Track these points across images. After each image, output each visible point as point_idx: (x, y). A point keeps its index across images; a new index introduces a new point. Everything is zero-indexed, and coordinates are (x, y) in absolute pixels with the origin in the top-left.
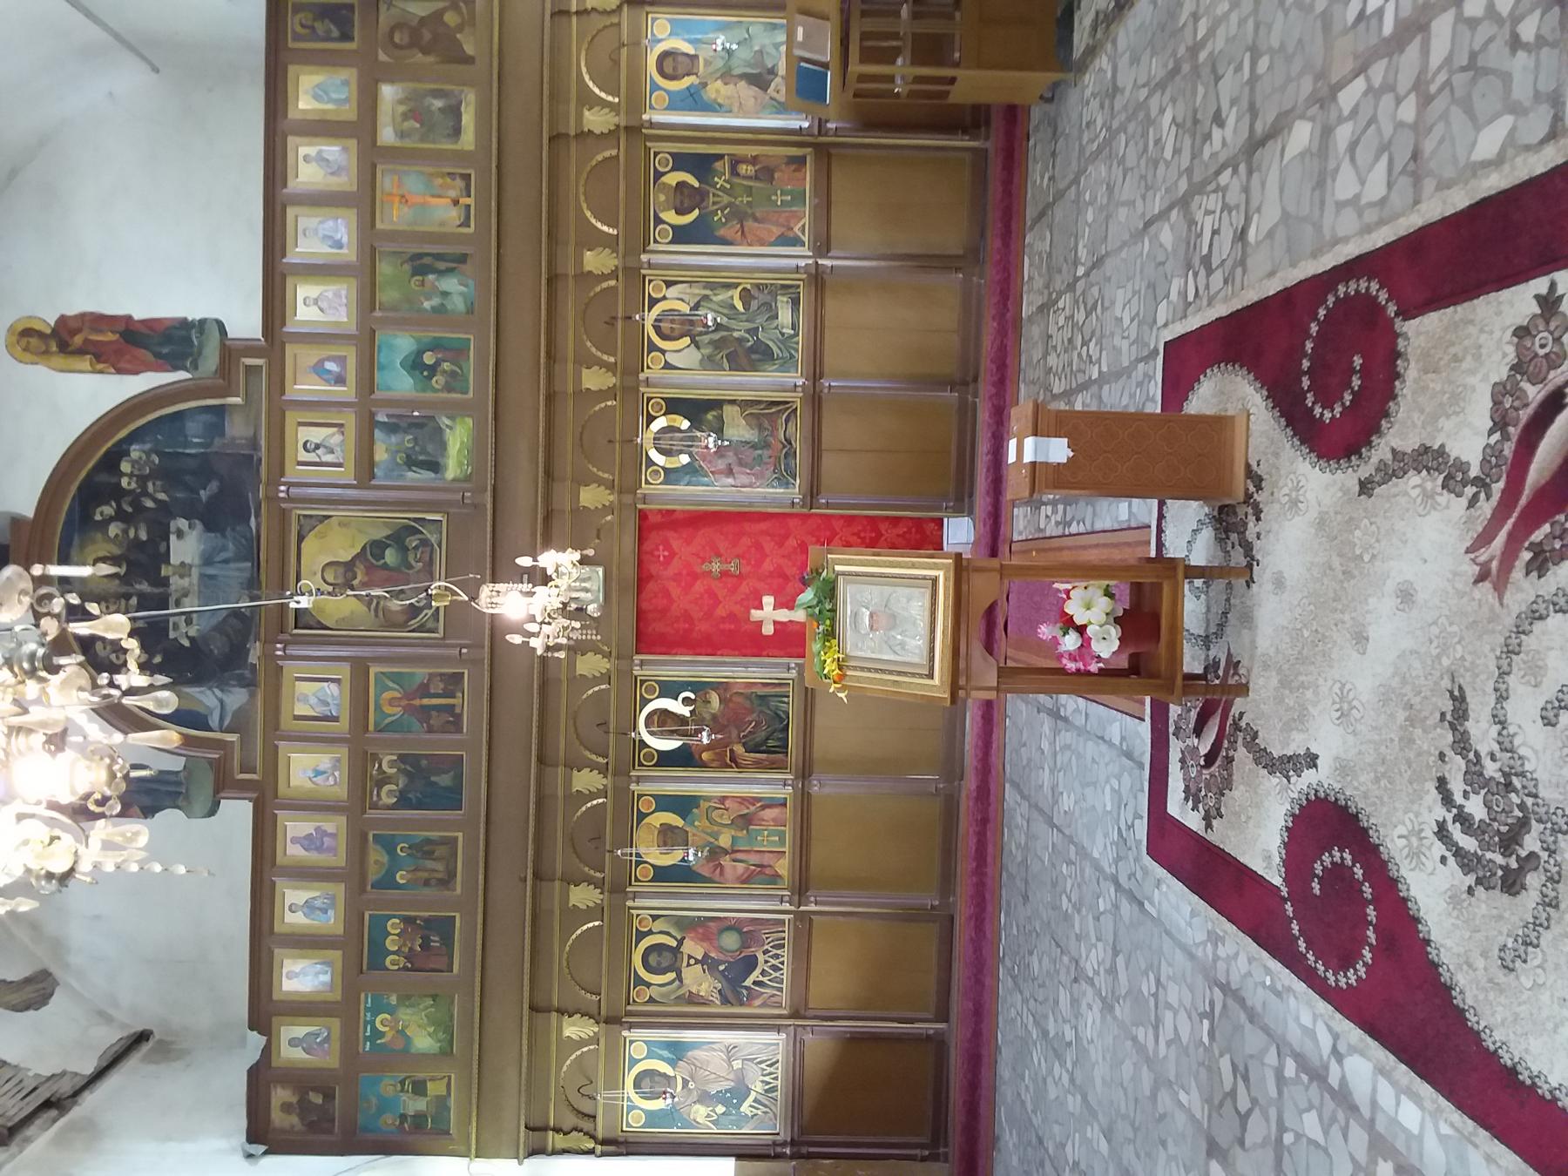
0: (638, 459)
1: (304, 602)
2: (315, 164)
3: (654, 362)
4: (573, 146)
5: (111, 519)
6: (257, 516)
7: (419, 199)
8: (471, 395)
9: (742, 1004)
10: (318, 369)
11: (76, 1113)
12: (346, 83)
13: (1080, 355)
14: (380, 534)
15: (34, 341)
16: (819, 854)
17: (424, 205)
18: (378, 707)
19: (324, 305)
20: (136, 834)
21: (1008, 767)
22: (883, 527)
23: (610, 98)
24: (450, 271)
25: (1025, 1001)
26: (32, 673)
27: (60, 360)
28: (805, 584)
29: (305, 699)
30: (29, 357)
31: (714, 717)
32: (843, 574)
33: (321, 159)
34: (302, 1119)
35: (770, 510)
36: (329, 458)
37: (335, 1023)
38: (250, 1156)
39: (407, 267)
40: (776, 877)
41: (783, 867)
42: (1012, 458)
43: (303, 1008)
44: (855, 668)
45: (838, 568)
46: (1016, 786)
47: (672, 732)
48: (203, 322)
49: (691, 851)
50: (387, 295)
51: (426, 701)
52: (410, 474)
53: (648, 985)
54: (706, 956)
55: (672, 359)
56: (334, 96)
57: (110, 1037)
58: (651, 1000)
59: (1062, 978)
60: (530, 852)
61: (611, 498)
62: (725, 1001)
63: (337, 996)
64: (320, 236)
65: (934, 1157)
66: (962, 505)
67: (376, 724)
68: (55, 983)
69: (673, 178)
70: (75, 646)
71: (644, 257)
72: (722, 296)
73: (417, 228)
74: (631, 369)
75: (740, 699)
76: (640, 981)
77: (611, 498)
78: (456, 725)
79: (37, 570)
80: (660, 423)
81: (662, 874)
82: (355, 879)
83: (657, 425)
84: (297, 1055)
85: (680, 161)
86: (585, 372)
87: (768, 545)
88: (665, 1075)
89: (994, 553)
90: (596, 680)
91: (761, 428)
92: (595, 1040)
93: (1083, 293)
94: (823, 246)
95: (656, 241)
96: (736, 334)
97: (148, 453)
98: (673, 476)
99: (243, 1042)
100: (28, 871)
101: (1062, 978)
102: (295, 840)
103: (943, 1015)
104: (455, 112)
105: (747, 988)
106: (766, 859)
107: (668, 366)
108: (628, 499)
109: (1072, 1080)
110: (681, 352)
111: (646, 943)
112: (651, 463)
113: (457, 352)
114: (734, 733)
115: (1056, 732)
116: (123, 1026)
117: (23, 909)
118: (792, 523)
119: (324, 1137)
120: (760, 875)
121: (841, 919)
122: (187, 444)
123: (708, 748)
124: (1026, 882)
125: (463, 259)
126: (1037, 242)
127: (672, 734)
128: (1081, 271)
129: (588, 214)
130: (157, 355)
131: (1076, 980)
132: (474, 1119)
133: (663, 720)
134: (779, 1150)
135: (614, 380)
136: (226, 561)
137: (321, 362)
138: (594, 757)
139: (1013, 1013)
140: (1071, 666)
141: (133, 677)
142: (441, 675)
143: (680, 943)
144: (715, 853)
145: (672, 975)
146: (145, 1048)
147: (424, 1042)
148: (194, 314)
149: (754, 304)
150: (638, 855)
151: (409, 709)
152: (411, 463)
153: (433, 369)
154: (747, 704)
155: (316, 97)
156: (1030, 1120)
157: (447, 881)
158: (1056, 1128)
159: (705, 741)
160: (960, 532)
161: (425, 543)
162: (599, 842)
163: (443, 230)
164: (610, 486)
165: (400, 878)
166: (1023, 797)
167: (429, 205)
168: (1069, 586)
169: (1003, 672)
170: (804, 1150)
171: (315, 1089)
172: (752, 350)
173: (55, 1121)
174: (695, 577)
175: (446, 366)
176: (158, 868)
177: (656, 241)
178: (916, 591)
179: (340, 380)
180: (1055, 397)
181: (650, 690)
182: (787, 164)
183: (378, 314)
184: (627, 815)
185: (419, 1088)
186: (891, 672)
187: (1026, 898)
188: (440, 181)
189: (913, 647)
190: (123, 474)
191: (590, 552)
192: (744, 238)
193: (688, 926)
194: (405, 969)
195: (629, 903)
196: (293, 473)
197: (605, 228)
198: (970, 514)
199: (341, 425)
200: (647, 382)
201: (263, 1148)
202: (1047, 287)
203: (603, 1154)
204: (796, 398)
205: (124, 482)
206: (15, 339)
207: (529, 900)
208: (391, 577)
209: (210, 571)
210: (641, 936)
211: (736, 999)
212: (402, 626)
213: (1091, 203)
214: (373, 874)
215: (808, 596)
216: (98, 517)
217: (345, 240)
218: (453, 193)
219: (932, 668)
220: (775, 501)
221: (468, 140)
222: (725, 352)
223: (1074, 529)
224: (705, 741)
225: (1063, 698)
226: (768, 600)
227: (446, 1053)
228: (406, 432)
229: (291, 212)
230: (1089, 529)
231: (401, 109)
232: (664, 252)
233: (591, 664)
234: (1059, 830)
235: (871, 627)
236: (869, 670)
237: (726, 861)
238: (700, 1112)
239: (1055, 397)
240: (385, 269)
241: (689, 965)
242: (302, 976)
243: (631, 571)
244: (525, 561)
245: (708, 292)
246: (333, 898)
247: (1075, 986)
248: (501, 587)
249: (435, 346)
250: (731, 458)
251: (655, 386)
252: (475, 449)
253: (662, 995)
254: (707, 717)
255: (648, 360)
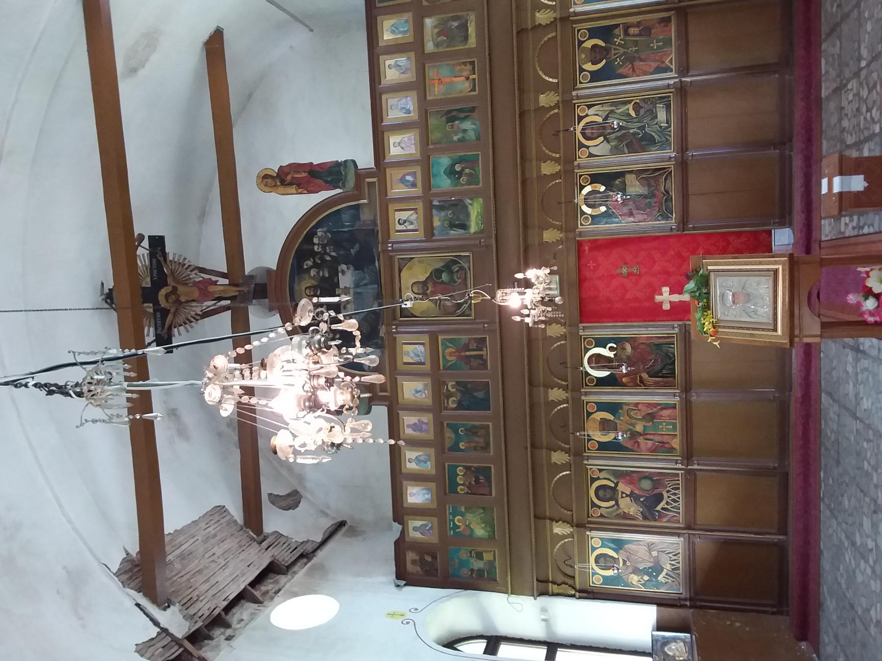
0: (574, 212)
1: (409, 304)
2: (394, 69)
3: (582, 154)
4: (530, 35)
5: (311, 267)
6: (379, 260)
7: (448, 80)
8: (481, 185)
9: (655, 520)
10: (403, 180)
11: (315, 560)
12: (407, 21)
13: (865, 118)
14: (439, 265)
15: (269, 181)
16: (698, 436)
17: (451, 82)
18: (444, 357)
19: (403, 145)
20: (367, 424)
21: (823, 383)
22: (731, 239)
23: (550, 3)
24: (466, 118)
25: (839, 524)
26: (319, 350)
27: (281, 189)
28: (689, 279)
29: (408, 354)
30: (268, 189)
31: (629, 358)
32: (714, 271)
33: (397, 66)
34: (422, 569)
35: (657, 234)
36: (411, 227)
37: (435, 520)
38: (398, 586)
39: (444, 118)
40: (672, 450)
41: (676, 443)
42: (824, 190)
43: (418, 512)
44: (724, 327)
45: (709, 268)
46: (830, 395)
47: (604, 367)
48: (346, 161)
49: (620, 434)
50: (435, 136)
51: (468, 353)
52: (452, 232)
53: (599, 507)
54: (632, 492)
55: (593, 151)
56: (402, 30)
57: (327, 524)
58: (602, 516)
59: (865, 510)
60: (528, 433)
61: (561, 235)
62: (645, 518)
63: (434, 506)
64: (400, 107)
65: (780, 613)
66: (784, 221)
67: (444, 366)
68: (301, 497)
69: (589, 44)
70: (300, 331)
71: (574, 93)
72: (622, 109)
73: (449, 96)
74: (569, 161)
75: (642, 346)
76: (594, 505)
77: (561, 235)
78: (484, 365)
79: (315, 300)
80: (588, 189)
81: (603, 446)
82: (441, 447)
83: (585, 191)
84: (417, 535)
85: (593, 33)
86: (543, 165)
87: (657, 255)
88: (612, 557)
89: (808, 251)
90: (558, 339)
91: (649, 186)
92: (571, 535)
93: (866, 78)
94: (684, 70)
95: (581, 83)
96: (631, 131)
97: (325, 232)
98: (597, 219)
99: (390, 528)
100: (323, 442)
101: (865, 510)
102: (408, 426)
103: (783, 529)
104: (464, 27)
105: (658, 511)
106: (665, 439)
107: (591, 155)
108: (571, 235)
109: (874, 572)
110: (599, 146)
111: (597, 484)
112: (583, 213)
113: (470, 162)
114: (641, 367)
115: (857, 360)
116: (333, 518)
117: (324, 461)
118: (672, 240)
119: (434, 578)
120: (662, 448)
121: (714, 474)
122: (343, 226)
123: (626, 375)
124: (838, 453)
125: (473, 109)
126: (830, 49)
127: (603, 368)
128: (863, 64)
129: (541, 73)
130: (326, 182)
131: (875, 512)
132: (509, 574)
133: (598, 361)
134: (682, 602)
135: (559, 167)
136: (366, 285)
137: (404, 176)
138: (559, 381)
139: (831, 531)
140: (871, 319)
141: (358, 350)
142: (475, 339)
143: (616, 484)
144: (634, 435)
145: (613, 503)
146: (344, 529)
147: (480, 532)
148: (341, 159)
149: (642, 112)
150: (588, 436)
151: (460, 358)
152: (452, 226)
153: (460, 174)
154: (648, 349)
155: (393, 32)
156: (845, 595)
157: (486, 447)
158: (863, 600)
159: (624, 371)
160: (783, 238)
161: (462, 268)
162: (567, 427)
163: (461, 95)
164: (560, 229)
165: (462, 445)
166: (834, 400)
167: (454, 82)
168: (868, 269)
169: (824, 325)
170: (698, 604)
171: (428, 554)
172: (641, 139)
173: (306, 564)
174: (613, 277)
175: (467, 171)
176: (371, 441)
177: (581, 83)
178: (763, 279)
179: (414, 185)
180: (848, 147)
181: (590, 343)
182: (659, 23)
183: (431, 147)
184: (580, 414)
185: (479, 556)
186: (748, 329)
187: (838, 462)
188: (459, 67)
189: (763, 313)
190: (315, 244)
191: (555, 268)
192: (634, 72)
193: (619, 475)
194: (467, 493)
195: (585, 462)
196: (395, 236)
197: (551, 80)
198: (790, 225)
199: (415, 209)
200: (579, 167)
201: (404, 582)
202: (838, 76)
203: (580, 598)
204: (671, 165)
205: (316, 248)
206: (261, 180)
207: (529, 459)
208: (445, 288)
209: (359, 290)
210: (593, 480)
211: (651, 515)
212: (453, 314)
213: (869, 18)
214: (448, 444)
215: (691, 285)
216: (305, 267)
217: (412, 109)
218: (466, 74)
219: (776, 325)
220: (660, 229)
221: (472, 41)
222: (625, 143)
223: (866, 230)
224: (624, 371)
225: (861, 340)
226: (666, 290)
227: (491, 538)
228: (448, 209)
229: (384, 97)
230: (877, 230)
231: (436, 30)
232: (586, 88)
233: (555, 330)
234: (861, 421)
235: (734, 302)
236: (733, 328)
237: (641, 439)
238: (634, 579)
239: (848, 147)
240: (433, 121)
241: (622, 497)
242: (416, 495)
243: (574, 276)
244: (519, 276)
245: (613, 108)
246: (429, 456)
247: (875, 516)
248: (508, 290)
249: (461, 160)
250: (631, 205)
251: (584, 168)
252: (485, 215)
253: (608, 513)
254: (624, 357)
255: (579, 153)
